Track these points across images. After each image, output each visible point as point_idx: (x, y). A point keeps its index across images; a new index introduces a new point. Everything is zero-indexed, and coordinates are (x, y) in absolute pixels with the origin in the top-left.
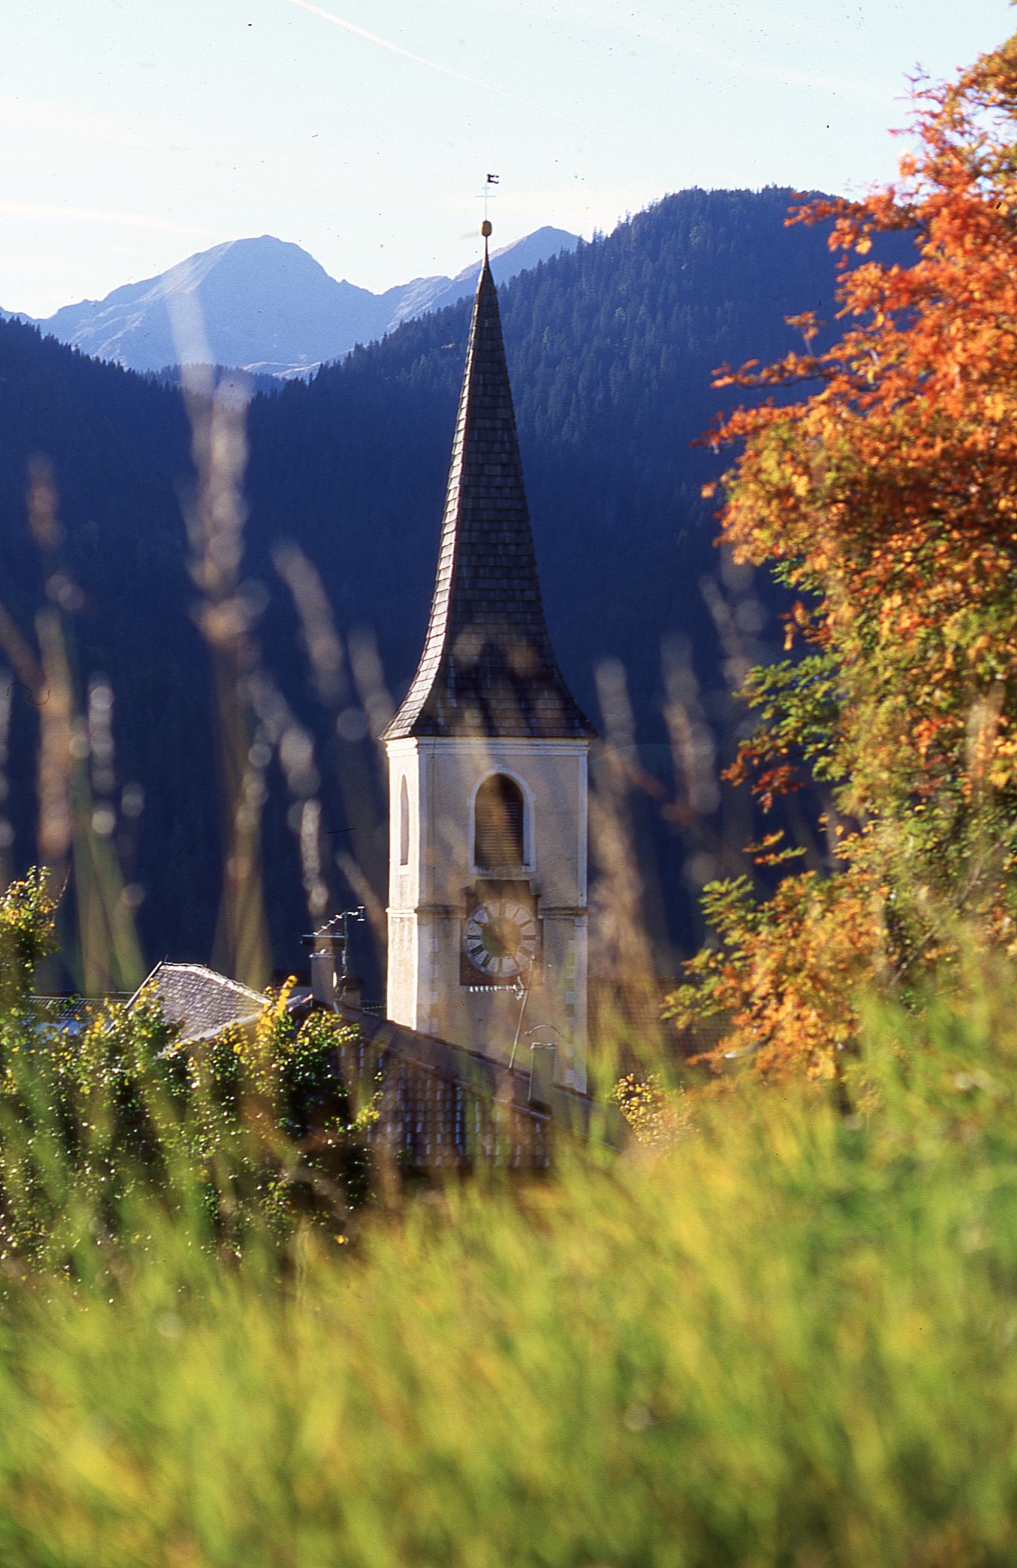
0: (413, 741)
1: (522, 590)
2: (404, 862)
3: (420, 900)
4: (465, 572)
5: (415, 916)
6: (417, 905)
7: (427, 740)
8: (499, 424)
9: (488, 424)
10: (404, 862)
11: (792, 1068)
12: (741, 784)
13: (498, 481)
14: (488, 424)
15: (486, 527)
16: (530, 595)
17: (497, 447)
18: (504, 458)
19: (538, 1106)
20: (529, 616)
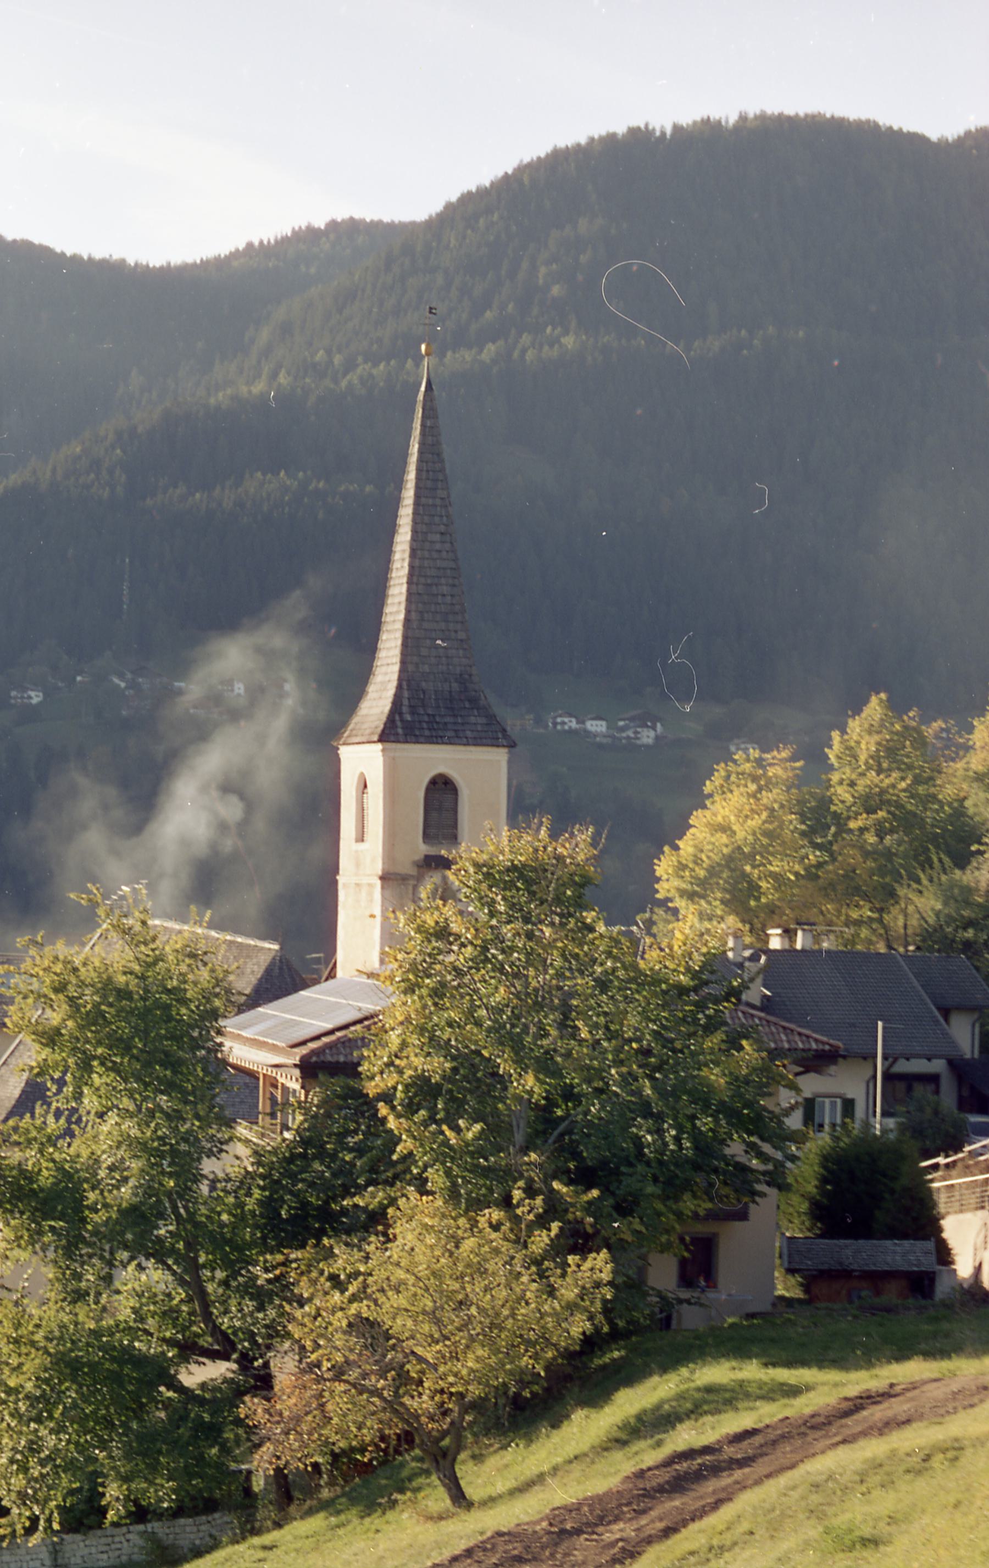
0: (379, 746)
1: (456, 632)
2: (361, 838)
3: (383, 870)
4: (414, 615)
5: (379, 883)
6: (380, 873)
7: (388, 745)
8: (438, 502)
9: (430, 501)
10: (361, 838)
11: (944, 878)
12: (773, 927)
13: (438, 546)
14: (430, 501)
15: (429, 581)
16: (462, 635)
17: (437, 519)
18: (442, 528)
19: (773, 912)
20: (461, 652)
